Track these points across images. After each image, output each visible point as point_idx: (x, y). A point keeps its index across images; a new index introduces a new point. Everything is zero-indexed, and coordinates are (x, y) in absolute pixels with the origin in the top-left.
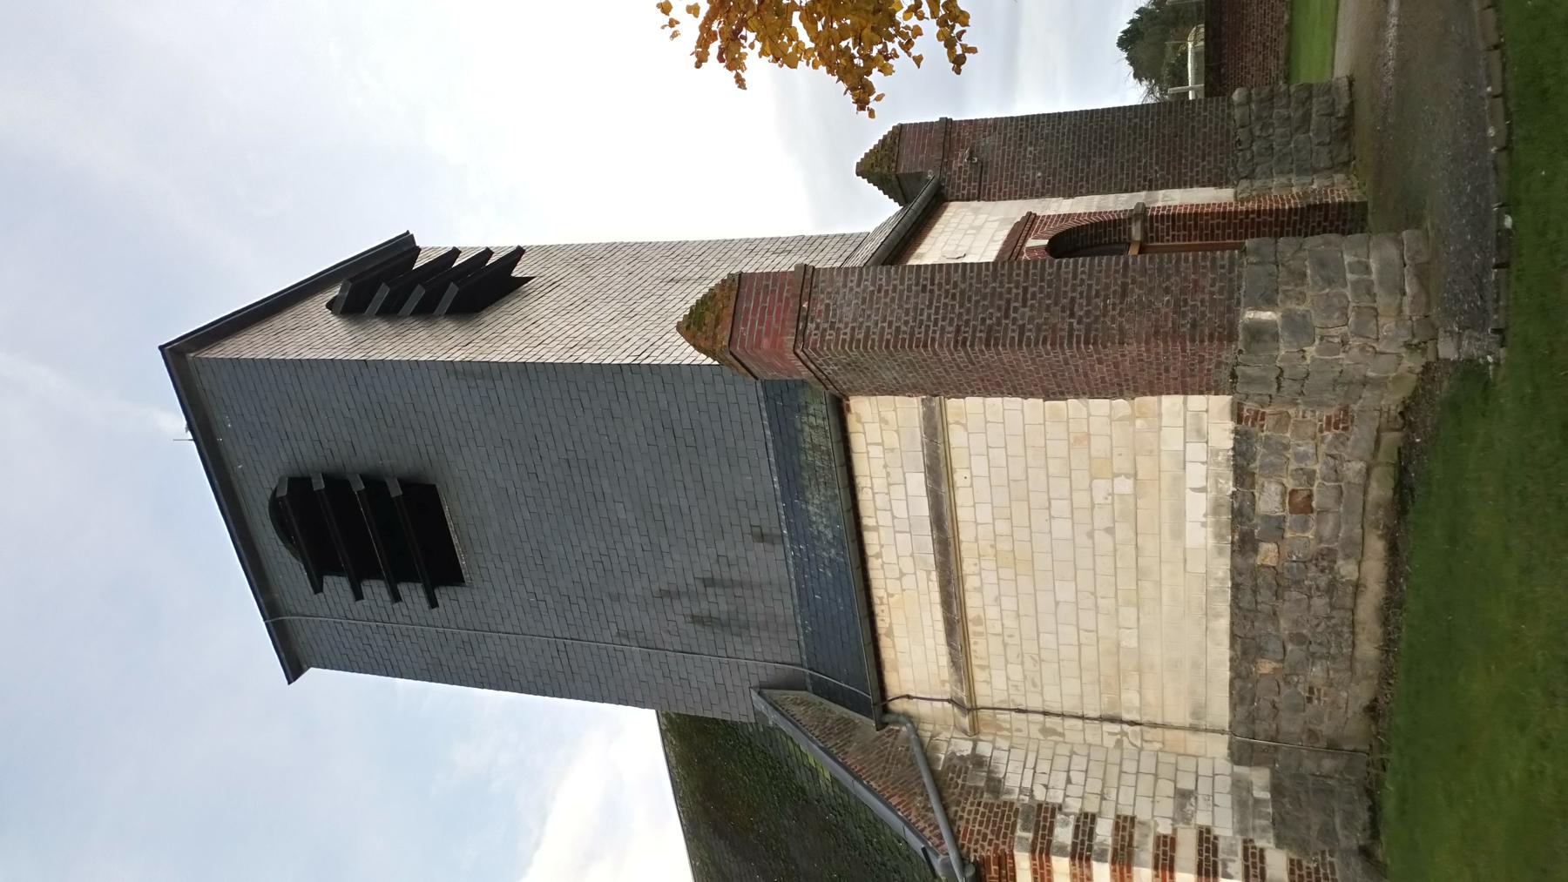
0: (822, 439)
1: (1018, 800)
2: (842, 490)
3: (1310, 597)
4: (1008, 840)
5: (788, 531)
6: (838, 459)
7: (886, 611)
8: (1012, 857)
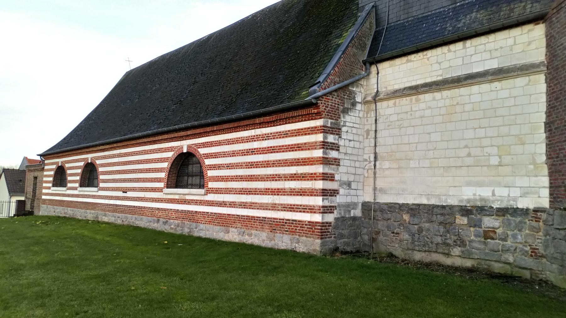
0: (517, 13)
1: (341, 120)
2: (501, 23)
3: (441, 236)
4: (326, 116)
5: (458, 6)
6: (506, 22)
7: (420, 58)
8: (321, 118)
